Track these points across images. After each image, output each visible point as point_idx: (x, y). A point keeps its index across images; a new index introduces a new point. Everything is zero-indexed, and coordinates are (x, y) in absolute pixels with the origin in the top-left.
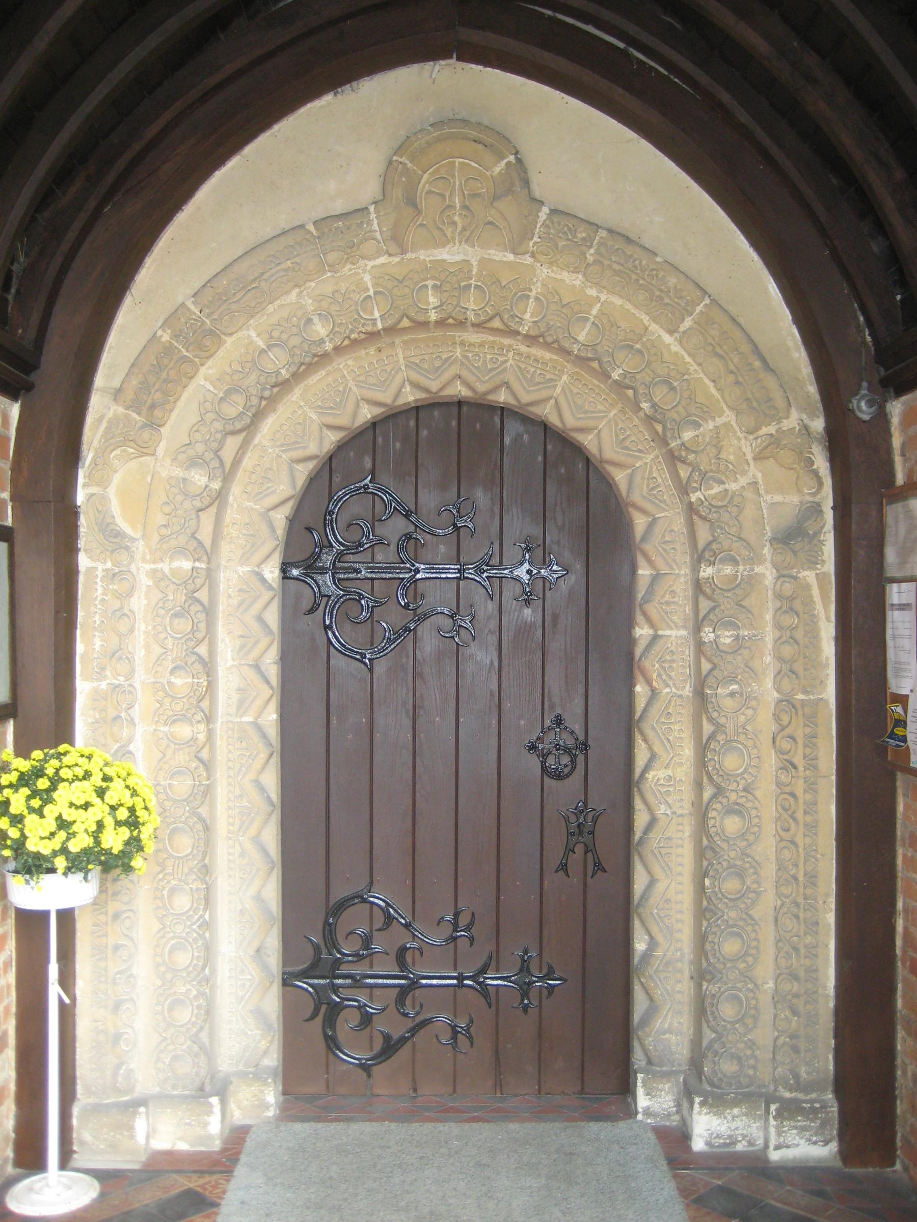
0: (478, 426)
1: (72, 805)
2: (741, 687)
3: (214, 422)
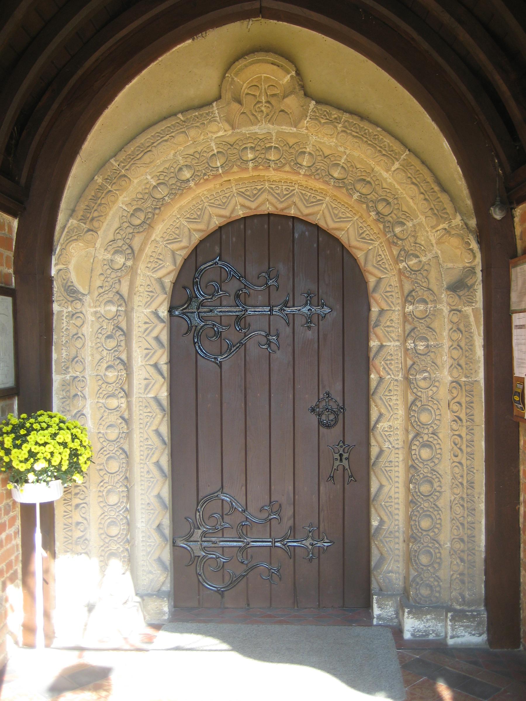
0: (280, 227)
1: (37, 443)
2: (430, 374)
3: (128, 228)
